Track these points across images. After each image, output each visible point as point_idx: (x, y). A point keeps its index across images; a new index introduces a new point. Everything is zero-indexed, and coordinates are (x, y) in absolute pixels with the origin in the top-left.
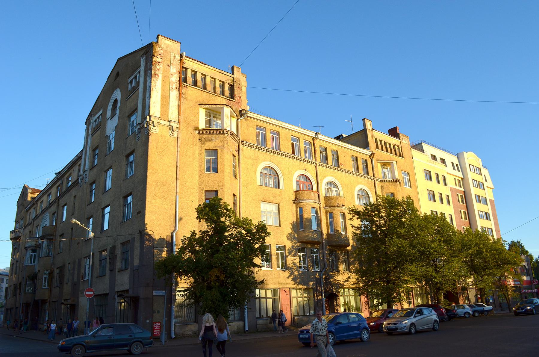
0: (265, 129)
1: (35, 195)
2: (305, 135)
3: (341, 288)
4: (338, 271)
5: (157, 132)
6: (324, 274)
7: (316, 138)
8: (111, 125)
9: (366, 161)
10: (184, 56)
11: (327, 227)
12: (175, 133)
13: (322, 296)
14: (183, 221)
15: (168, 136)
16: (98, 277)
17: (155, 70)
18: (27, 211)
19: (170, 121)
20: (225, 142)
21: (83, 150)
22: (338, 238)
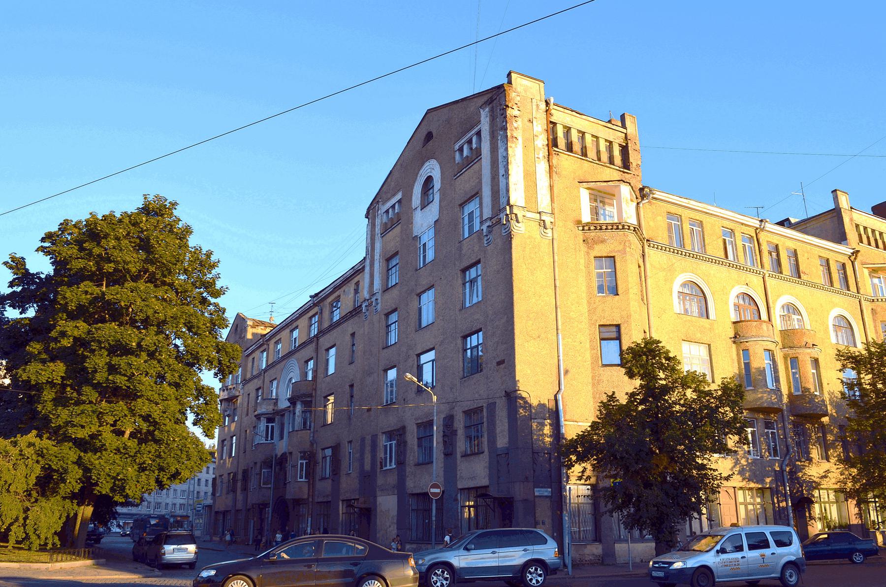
0: (680, 218)
1: (261, 330)
2: (742, 224)
3: (815, 488)
4: (810, 460)
5: (524, 232)
6: (787, 465)
7: (763, 230)
8: (424, 222)
9: (844, 265)
10: (552, 104)
11: (789, 382)
12: (549, 231)
13: (786, 501)
14: (569, 375)
15: (538, 236)
16: (418, 465)
17: (512, 130)
18: (248, 356)
19: (540, 213)
20: (627, 244)
21: (365, 258)
22: (809, 402)
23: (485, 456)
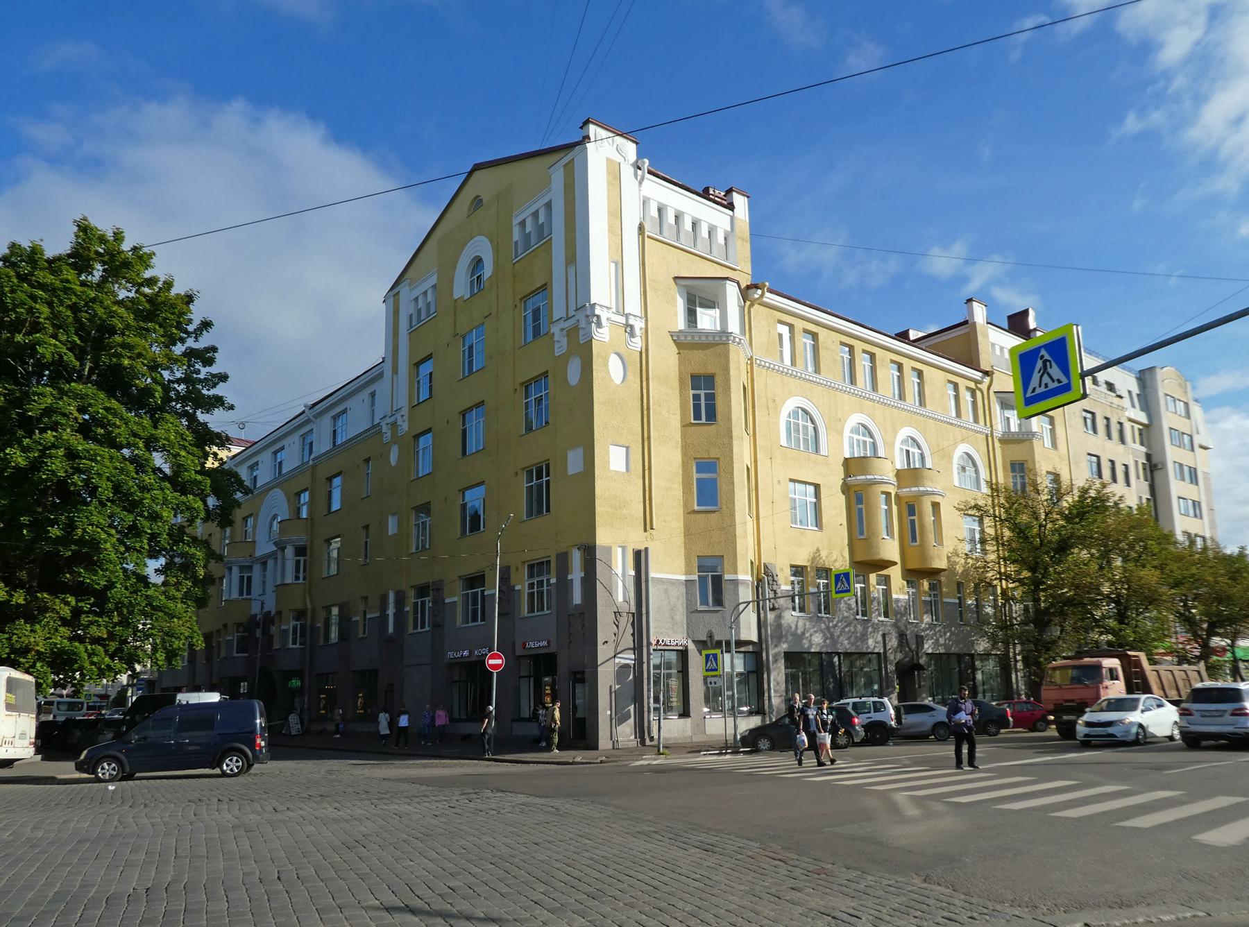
23: (1124, 696)
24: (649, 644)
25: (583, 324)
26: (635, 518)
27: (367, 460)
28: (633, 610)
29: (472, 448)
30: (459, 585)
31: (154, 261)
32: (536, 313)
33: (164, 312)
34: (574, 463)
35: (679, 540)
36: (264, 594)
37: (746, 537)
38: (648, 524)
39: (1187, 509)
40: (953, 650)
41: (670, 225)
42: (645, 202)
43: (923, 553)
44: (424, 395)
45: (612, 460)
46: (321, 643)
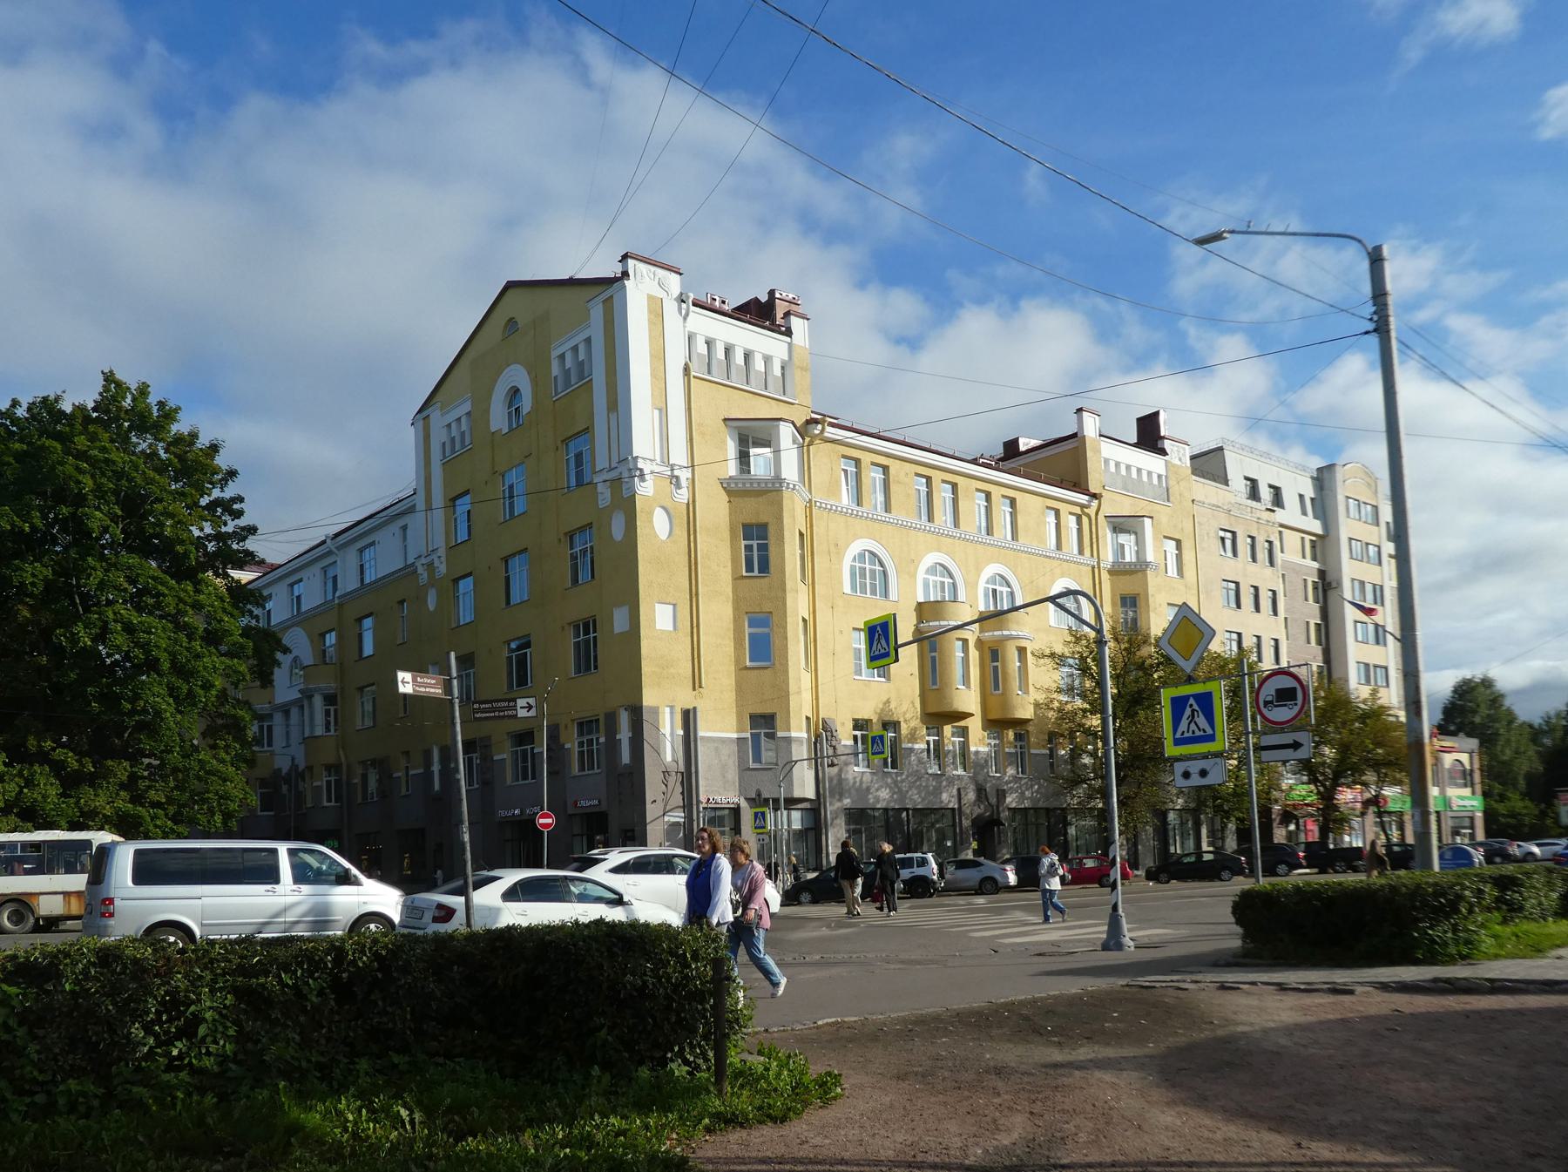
24: (698, 802)
25: (625, 474)
26: (684, 677)
27: (402, 602)
28: (682, 768)
29: (516, 597)
30: (508, 744)
31: (180, 416)
32: (579, 456)
33: (195, 465)
34: (620, 622)
35: (730, 697)
36: (288, 746)
37: (799, 693)
38: (696, 683)
39: (1366, 633)
40: (1041, 805)
41: (719, 361)
42: (691, 338)
43: (1005, 702)
44: (462, 535)
45: (659, 619)
46: (360, 800)
